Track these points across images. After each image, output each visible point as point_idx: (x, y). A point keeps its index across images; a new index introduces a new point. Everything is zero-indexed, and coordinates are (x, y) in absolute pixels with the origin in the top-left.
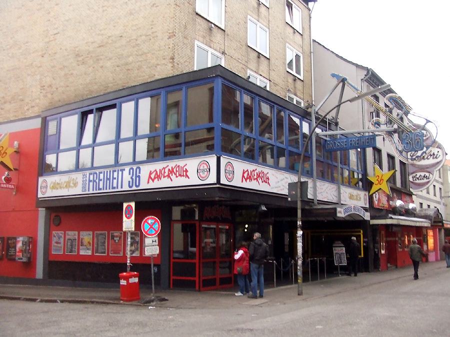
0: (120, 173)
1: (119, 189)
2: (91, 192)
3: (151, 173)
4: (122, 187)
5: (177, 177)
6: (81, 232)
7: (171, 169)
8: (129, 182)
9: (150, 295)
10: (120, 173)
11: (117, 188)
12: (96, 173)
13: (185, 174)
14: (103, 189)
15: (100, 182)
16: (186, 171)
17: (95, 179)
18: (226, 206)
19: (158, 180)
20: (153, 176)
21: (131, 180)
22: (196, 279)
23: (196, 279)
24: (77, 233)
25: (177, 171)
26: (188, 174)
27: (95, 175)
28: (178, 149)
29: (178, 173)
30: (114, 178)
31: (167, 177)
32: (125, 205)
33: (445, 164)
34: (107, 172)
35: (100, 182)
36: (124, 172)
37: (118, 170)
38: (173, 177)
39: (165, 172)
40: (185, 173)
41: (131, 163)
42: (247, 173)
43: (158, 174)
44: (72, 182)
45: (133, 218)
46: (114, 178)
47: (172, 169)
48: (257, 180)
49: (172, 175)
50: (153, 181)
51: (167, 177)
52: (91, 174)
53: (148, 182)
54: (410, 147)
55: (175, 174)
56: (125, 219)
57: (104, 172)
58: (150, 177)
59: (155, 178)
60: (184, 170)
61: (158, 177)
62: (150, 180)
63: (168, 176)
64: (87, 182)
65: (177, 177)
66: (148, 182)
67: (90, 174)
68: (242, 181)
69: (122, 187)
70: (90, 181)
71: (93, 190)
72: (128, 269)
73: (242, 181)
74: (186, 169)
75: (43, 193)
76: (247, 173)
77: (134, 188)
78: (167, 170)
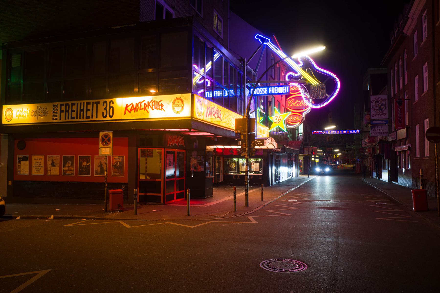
0: (95, 106)
1: (94, 119)
3: (127, 106)
4: (97, 117)
5: (153, 109)
6: (240, 171)
7: (147, 104)
8: (103, 113)
10: (95, 106)
11: (92, 118)
12: (68, 105)
14: (77, 118)
16: (162, 105)
17: (67, 109)
19: (135, 112)
20: (129, 108)
21: (105, 111)
22: (162, 195)
23: (162, 195)
24: (42, 157)
25: (152, 105)
26: (163, 107)
28: (40, 161)
30: (88, 110)
31: (143, 110)
32: (101, 134)
34: (81, 103)
36: (99, 105)
37: (93, 103)
39: (141, 106)
40: (160, 107)
41: (97, 105)
47: (149, 104)
48: (215, 116)
49: (148, 108)
50: (130, 112)
51: (143, 110)
52: (63, 105)
53: (125, 113)
54: (316, 94)
55: (152, 108)
56: (101, 145)
57: (78, 104)
59: (131, 110)
60: (160, 104)
62: (127, 111)
66: (125, 113)
67: (61, 105)
68: (207, 117)
69: (97, 117)
71: (65, 119)
73: (207, 117)
75: (8, 120)
78: (143, 104)
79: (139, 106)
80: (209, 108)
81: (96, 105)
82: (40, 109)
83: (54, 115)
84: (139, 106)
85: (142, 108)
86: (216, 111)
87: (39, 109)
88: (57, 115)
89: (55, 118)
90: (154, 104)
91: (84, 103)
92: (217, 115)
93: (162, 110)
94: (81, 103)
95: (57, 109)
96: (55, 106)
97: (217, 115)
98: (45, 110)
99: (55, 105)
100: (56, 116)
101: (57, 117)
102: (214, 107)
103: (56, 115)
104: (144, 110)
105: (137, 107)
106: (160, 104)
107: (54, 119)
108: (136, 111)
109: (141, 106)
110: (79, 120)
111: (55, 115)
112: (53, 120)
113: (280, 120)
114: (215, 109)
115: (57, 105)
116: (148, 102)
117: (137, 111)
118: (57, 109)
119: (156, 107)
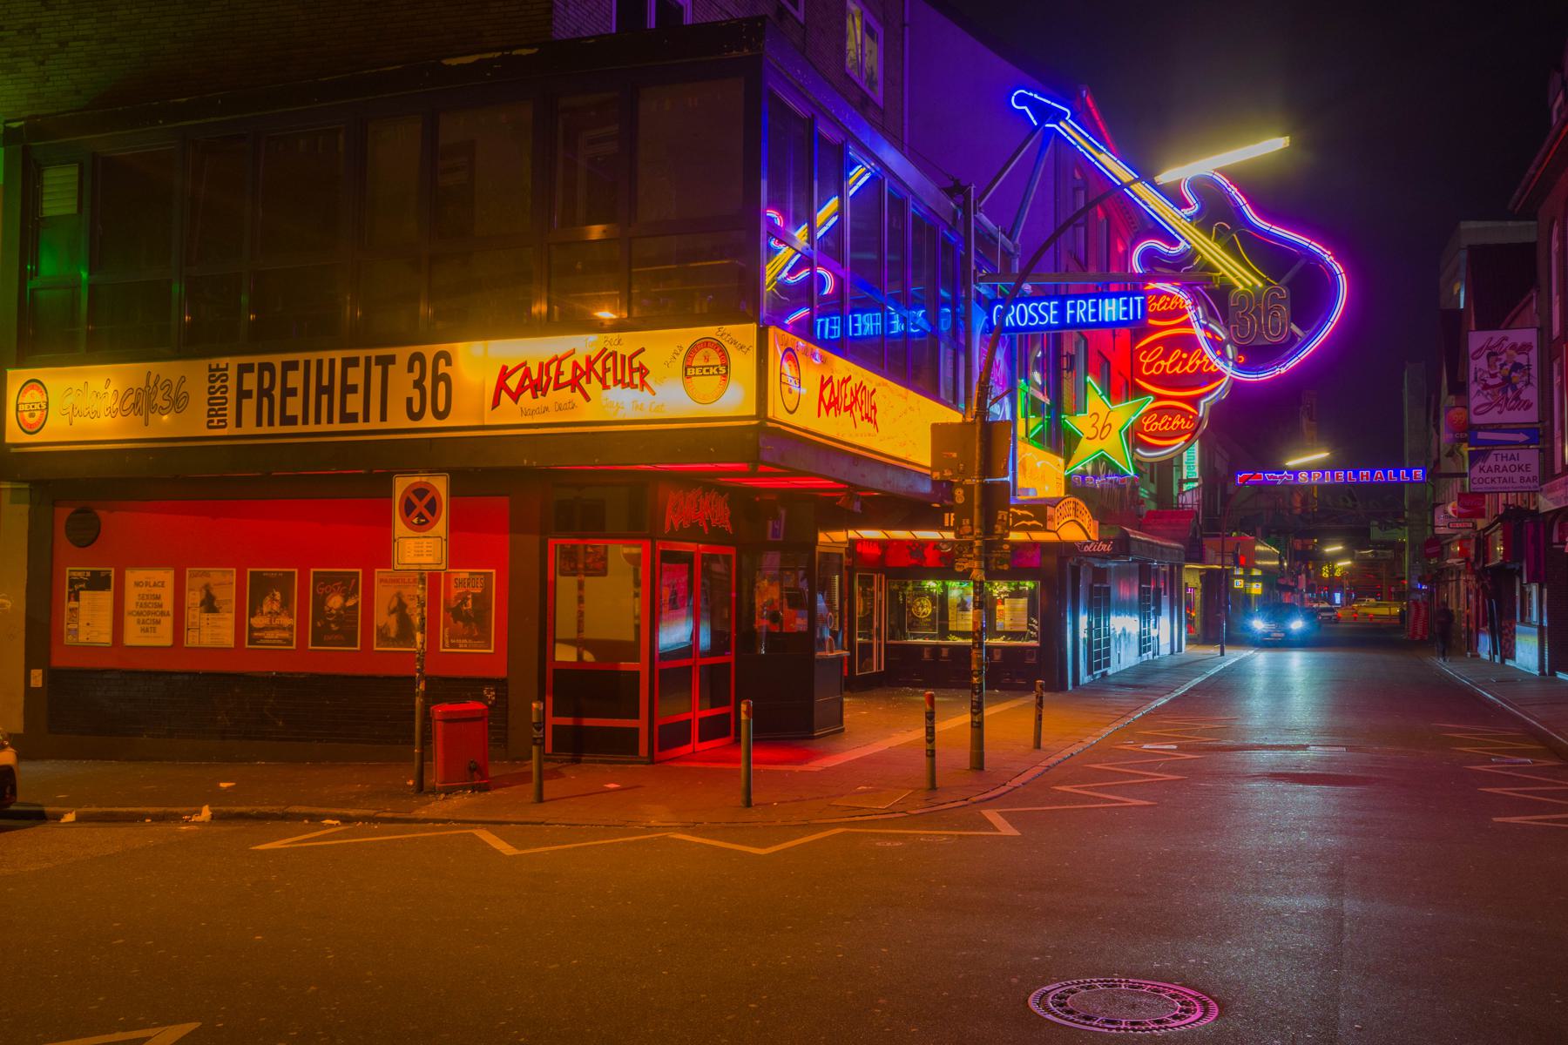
0: (376, 371)
1: (375, 423)
2: (249, 427)
3: (504, 374)
4: (383, 418)
5: (606, 387)
8: (410, 401)
9: (1452, 611)
10: (376, 371)
11: (366, 419)
13: (637, 381)
14: (305, 422)
15: (245, 402)
17: (266, 385)
18: (722, 490)
19: (535, 396)
20: (513, 383)
21: (416, 394)
25: (605, 370)
27: (267, 375)
29: (610, 376)
30: (348, 389)
32: (401, 485)
33: (211, 573)
34: (320, 363)
35: (245, 402)
36: (391, 367)
37: (368, 359)
38: (593, 387)
39: (559, 373)
40: (636, 376)
42: (830, 386)
43: (535, 376)
44: (160, 393)
45: (441, 526)
46: (348, 389)
49: (589, 381)
50: (515, 397)
55: (603, 380)
56: (399, 527)
57: (307, 363)
58: (501, 385)
59: (521, 388)
60: (636, 364)
61: (538, 388)
62: (504, 394)
63: (574, 383)
64: (232, 395)
65: (606, 387)
66: (496, 402)
67: (243, 369)
68: (819, 415)
69: (383, 418)
70: (243, 394)
71: (259, 423)
72: (871, 641)
73: (819, 415)
74: (641, 364)
76: (829, 386)
77: (429, 421)
78: (567, 367)
79: (552, 373)
80: (830, 380)
81: (379, 368)
82: (158, 385)
83: (213, 410)
84: (552, 373)
85: (562, 379)
86: (857, 392)
87: (152, 384)
88: (225, 409)
89: (216, 419)
90: (609, 363)
91: (332, 362)
92: (861, 409)
93: (642, 390)
94: (320, 363)
95: (227, 383)
96: (218, 374)
97: (861, 409)
98: (177, 391)
99: (218, 369)
100: (220, 412)
101: (225, 415)
102: (850, 378)
103: (220, 409)
104: (573, 390)
105: (545, 378)
107: (215, 424)
108: (539, 393)
110: (312, 427)
111: (216, 408)
112: (210, 427)
113: (1107, 428)
114: (850, 384)
115: (226, 369)
116: (588, 358)
117: (544, 394)
118: (227, 383)
119: (619, 377)
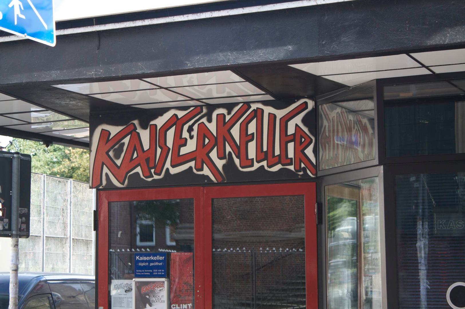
25: (246, 137)
29: (252, 147)
40: (291, 146)
79: (170, 143)
84: (170, 143)
90: (252, 128)
106: (291, 130)
109: (179, 142)
